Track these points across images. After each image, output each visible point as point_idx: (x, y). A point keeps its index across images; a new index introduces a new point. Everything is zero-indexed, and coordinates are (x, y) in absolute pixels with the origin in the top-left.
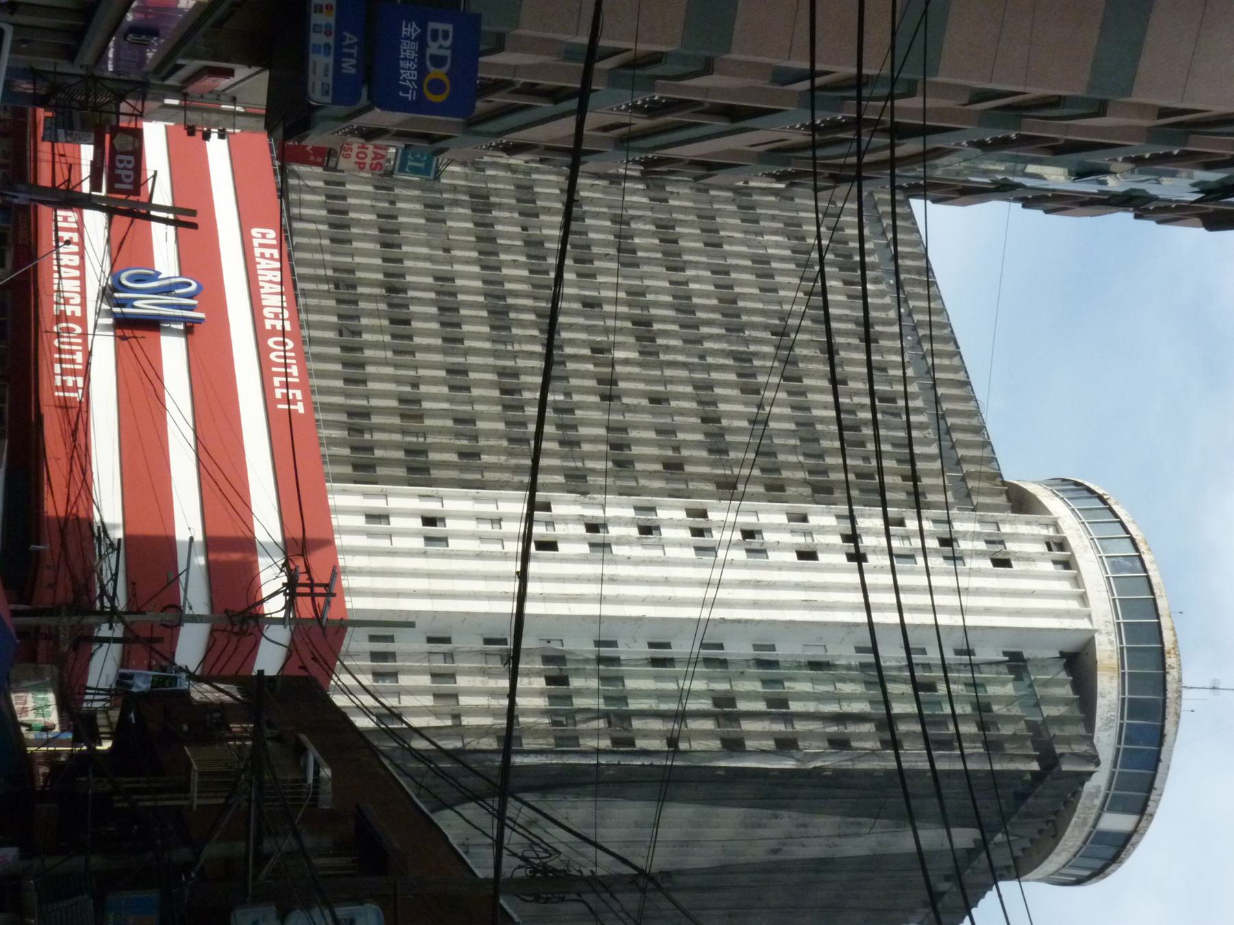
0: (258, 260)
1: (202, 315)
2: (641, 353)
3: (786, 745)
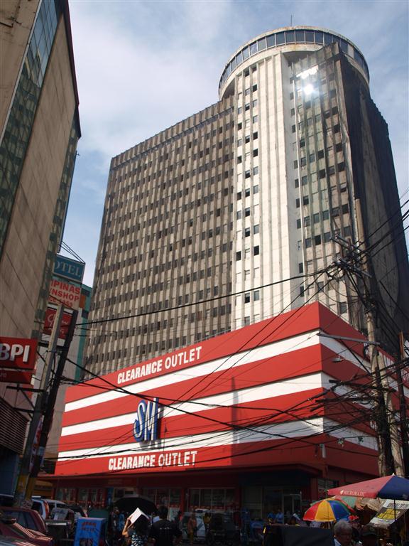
2: (172, 233)
3: (339, 148)
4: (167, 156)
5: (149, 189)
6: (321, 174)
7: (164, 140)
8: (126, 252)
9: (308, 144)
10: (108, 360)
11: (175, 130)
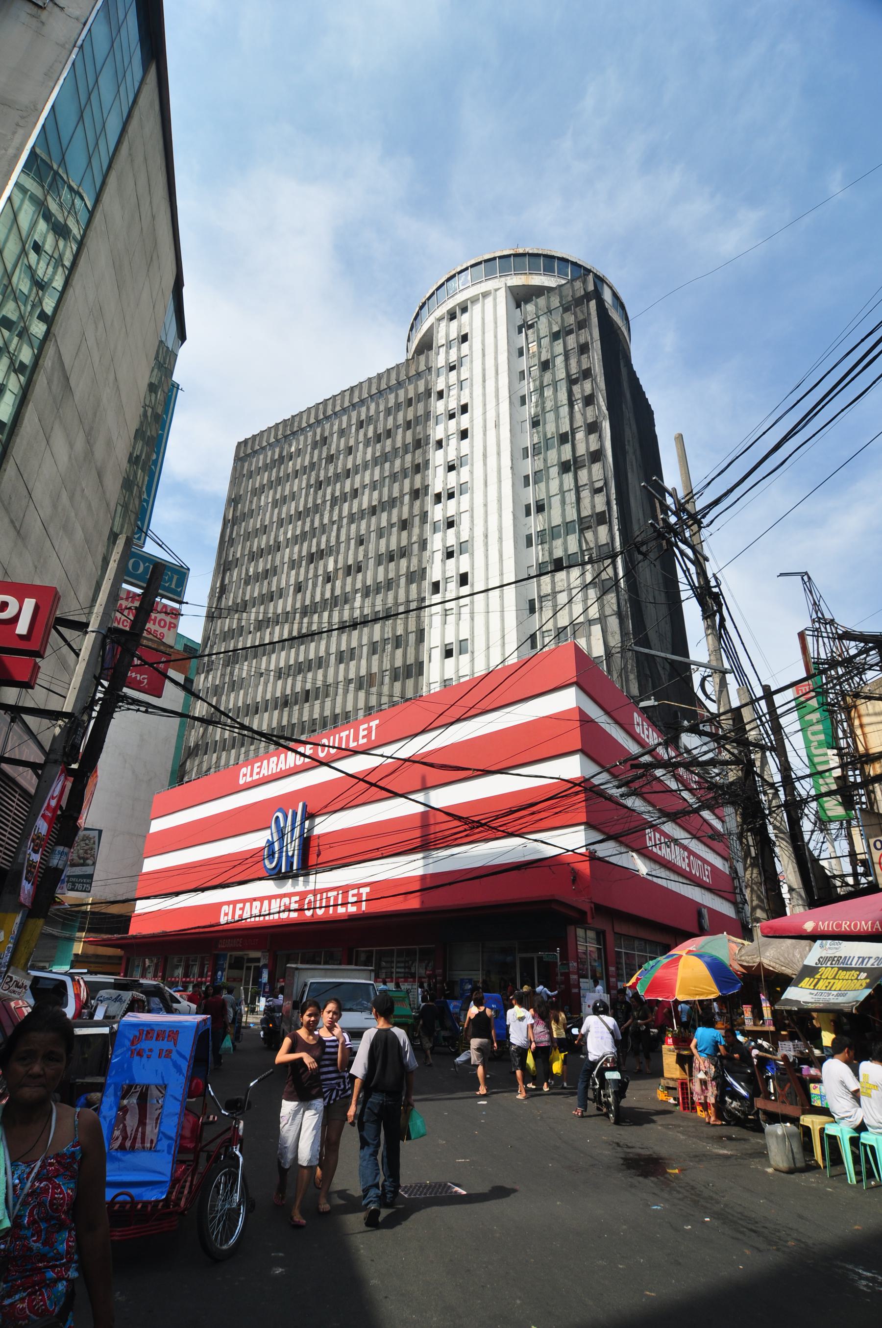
0: (261, 776)
1: (301, 805)
4: (324, 440)
5: (295, 489)
6: (565, 467)
7: (321, 416)
8: (258, 584)
9: (545, 424)
10: (224, 750)
11: (338, 402)
